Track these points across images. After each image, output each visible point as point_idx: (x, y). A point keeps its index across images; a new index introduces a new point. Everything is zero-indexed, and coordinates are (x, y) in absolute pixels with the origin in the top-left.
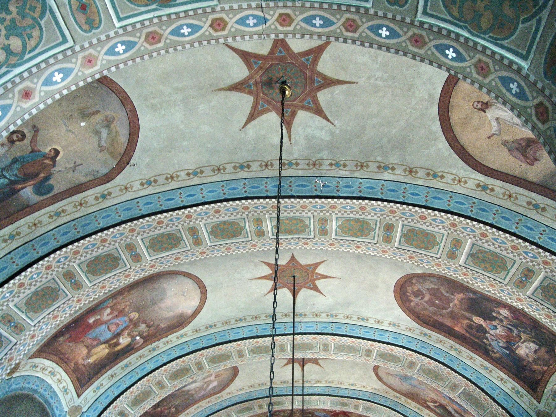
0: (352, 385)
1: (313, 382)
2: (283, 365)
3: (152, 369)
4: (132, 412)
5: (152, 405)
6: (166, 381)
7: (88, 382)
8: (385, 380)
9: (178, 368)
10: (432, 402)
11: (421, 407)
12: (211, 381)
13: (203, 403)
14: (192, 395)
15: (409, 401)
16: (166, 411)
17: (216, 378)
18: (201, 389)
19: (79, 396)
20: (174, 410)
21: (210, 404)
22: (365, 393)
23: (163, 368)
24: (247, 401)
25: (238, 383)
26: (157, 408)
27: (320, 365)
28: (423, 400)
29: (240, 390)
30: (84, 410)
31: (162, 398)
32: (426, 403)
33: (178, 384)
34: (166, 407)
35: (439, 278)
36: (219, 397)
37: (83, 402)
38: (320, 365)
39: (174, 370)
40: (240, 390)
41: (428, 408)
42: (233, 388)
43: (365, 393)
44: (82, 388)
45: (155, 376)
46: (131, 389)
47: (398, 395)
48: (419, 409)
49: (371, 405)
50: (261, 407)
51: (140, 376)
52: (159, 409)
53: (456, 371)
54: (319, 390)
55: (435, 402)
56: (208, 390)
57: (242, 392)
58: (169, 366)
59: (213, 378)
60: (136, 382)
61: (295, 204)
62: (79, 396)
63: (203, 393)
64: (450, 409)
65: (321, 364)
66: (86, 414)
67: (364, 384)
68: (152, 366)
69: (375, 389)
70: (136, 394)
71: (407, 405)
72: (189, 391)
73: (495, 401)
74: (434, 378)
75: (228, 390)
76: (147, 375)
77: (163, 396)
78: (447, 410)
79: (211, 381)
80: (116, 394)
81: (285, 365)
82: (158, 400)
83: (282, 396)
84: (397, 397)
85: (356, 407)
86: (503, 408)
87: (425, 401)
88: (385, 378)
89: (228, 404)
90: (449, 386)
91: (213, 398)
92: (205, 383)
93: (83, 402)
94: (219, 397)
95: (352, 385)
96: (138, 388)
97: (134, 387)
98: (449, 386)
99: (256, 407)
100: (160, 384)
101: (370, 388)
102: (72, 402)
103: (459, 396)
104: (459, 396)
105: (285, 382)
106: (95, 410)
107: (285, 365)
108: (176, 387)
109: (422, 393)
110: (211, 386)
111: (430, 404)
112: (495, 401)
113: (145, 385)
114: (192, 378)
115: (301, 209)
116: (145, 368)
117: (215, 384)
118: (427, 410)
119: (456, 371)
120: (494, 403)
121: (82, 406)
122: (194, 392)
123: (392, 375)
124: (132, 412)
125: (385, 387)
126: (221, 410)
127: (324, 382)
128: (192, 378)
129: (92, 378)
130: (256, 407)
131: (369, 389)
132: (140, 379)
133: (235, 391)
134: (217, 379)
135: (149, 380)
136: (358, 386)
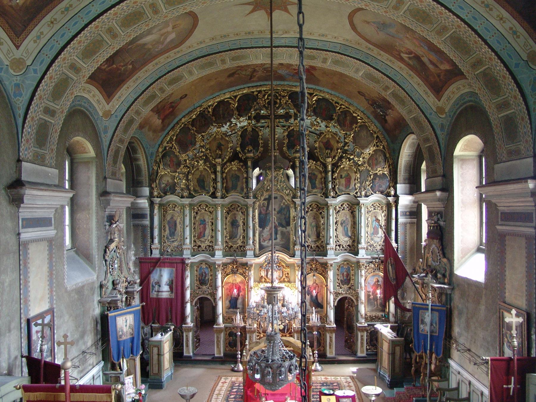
0: (323, 35)
1: (280, 33)
2: (247, 12)
3: (99, 12)
4: (85, 66)
5: (106, 58)
6: (118, 28)
7: (24, 30)
8: (359, 30)
9: (130, 11)
10: (406, 53)
11: (393, 59)
12: (168, 33)
13: (162, 59)
14: (149, 50)
15: (382, 53)
16: (123, 69)
17: (173, 28)
18: (158, 42)
19: (18, 47)
20: (131, 67)
21: (169, 60)
22: (336, 45)
23: (112, 11)
24: (209, 55)
25: (198, 35)
26: (112, 65)
27: (288, 12)
28: (397, 50)
29: (201, 43)
30: (29, 63)
31: (116, 50)
32: (400, 55)
33: (132, 32)
34: (122, 64)
35: (174, 108)
36: (178, 52)
37: (24, 54)
38: (288, 12)
39: (126, 13)
40: (201, 43)
41: (401, 60)
42: (192, 41)
43: (336, 45)
44: (18, 38)
45: (104, 22)
46: (78, 38)
47: (371, 46)
48: (390, 61)
49: (341, 58)
50: (223, 61)
51: (86, 22)
52: (114, 66)
53: (450, 11)
54: (287, 41)
55: (410, 53)
56: (166, 43)
57: (203, 45)
58: (118, 8)
59: (170, 29)
60: (83, 29)
61: (109, 15)
62: (18, 47)
63: (161, 47)
64: (425, 60)
65: (290, 11)
66: (31, 67)
67: (336, 35)
68: (99, 10)
69: (347, 40)
70: (85, 44)
71: (379, 58)
72: (145, 44)
73: (486, 43)
74: (421, 20)
75: (188, 43)
76: (94, 20)
77: (117, 47)
78: (422, 61)
79: (168, 33)
80: (62, 44)
81: (249, 13)
82: (111, 52)
83: (246, 48)
84: (370, 49)
85: (325, 61)
86: (493, 50)
87: (400, 52)
88: (360, 26)
89: (188, 58)
90: (436, 30)
91: (171, 53)
92: (162, 35)
93: (24, 54)
94: (178, 52)
95: (323, 35)
96: (86, 36)
97: (82, 35)
98: (436, 30)
99: (219, 63)
100: (110, 32)
101: (341, 39)
102: (11, 54)
103: (445, 42)
104: (445, 42)
105: (249, 33)
106: (41, 63)
107: (249, 13)
108: (130, 36)
109: (397, 44)
110: (168, 40)
111: (404, 56)
112: (486, 43)
113: (94, 33)
114: (148, 25)
115: (114, 16)
116: (90, 11)
117: (173, 36)
118: (399, 63)
119: (450, 11)
120: (484, 45)
121: (25, 59)
122: (150, 47)
123: (368, 23)
124: (85, 66)
125: (358, 37)
126: (182, 65)
127: (292, 33)
128: (148, 25)
129: (28, 25)
130: (219, 63)
131: (340, 40)
132: (86, 26)
133: (195, 45)
134: (175, 29)
135: (97, 27)
136: (329, 37)
